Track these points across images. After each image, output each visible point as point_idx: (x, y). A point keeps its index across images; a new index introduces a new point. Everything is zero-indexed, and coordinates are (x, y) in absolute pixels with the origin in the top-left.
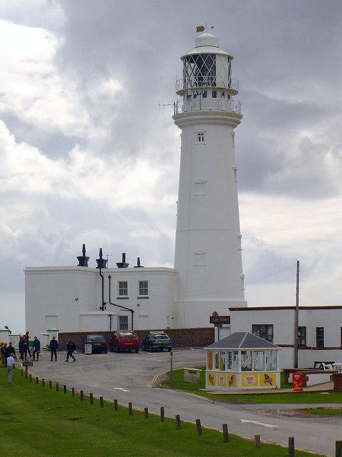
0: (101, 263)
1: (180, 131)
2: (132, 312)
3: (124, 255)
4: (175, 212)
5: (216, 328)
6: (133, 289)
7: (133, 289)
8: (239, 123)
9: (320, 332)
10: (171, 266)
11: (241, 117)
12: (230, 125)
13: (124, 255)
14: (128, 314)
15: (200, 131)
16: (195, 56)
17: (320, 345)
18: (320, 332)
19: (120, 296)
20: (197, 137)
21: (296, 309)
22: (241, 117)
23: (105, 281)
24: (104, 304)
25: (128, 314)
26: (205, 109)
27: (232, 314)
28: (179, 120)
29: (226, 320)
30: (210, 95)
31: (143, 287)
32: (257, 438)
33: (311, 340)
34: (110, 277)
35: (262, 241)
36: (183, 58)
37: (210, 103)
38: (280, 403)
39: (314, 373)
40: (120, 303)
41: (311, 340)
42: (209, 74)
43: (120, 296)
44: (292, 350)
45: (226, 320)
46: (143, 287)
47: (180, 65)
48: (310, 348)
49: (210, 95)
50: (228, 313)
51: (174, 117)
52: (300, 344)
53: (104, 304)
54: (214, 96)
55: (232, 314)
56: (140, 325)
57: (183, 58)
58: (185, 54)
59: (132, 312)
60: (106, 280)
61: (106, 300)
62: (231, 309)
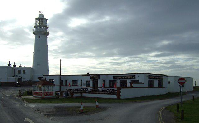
3: (21, 65)
6: (22, 72)
7: (22, 72)
10: (31, 66)
12: (46, 35)
13: (21, 65)
14: (20, 78)
17: (66, 85)
18: (66, 81)
21: (60, 75)
24: (15, 75)
31: (24, 72)
32: (88, 73)
33: (64, 83)
35: (48, 34)
38: (44, 103)
40: (19, 75)
41: (64, 83)
44: (59, 86)
47: (35, 20)
48: (134, 88)
51: (33, 32)
52: (61, 85)
53: (15, 75)
56: (23, 80)
60: (15, 70)
61: (15, 74)
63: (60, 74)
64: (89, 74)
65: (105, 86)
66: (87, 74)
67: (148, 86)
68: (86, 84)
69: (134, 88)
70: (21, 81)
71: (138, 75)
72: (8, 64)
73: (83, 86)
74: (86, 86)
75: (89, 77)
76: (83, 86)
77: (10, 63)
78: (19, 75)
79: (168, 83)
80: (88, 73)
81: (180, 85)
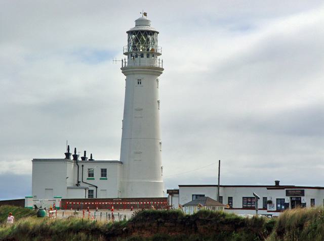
0: (75, 157)
1: (125, 77)
2: (97, 187)
4: (32, 170)
5: (170, 196)
6: (97, 174)
8: (161, 73)
9: (230, 199)
11: (163, 69)
14: (91, 188)
15: (139, 78)
16: (137, 32)
18: (230, 199)
19: (102, 178)
20: (137, 81)
21: (218, 186)
22: (163, 69)
23: (79, 169)
24: (79, 182)
25: (94, 189)
26: (142, 64)
27: (181, 189)
28: (125, 70)
29: (177, 192)
30: (145, 56)
31: (104, 173)
34: (83, 166)
36: (127, 32)
37: (145, 62)
39: (111, 200)
40: (89, 182)
42: (145, 43)
43: (102, 178)
45: (177, 192)
46: (104, 173)
47: (32, 162)
48: (234, 209)
49: (145, 56)
50: (178, 188)
53: (79, 182)
54: (148, 56)
55: (181, 189)
57: (127, 32)
58: (129, 30)
59: (97, 187)
61: (80, 180)
62: (180, 186)
63: (217, 184)
64: (280, 184)
65: (233, 207)
66: (274, 184)
67: (262, 208)
68: (290, 204)
69: (234, 209)
70: (95, 197)
71: (6, 206)
72: (65, 154)
73: (268, 209)
74: (275, 210)
75: (284, 191)
76: (268, 209)
77: (77, 154)
78: (89, 182)
79: (314, 200)
80: (277, 182)
81: (52, 207)
